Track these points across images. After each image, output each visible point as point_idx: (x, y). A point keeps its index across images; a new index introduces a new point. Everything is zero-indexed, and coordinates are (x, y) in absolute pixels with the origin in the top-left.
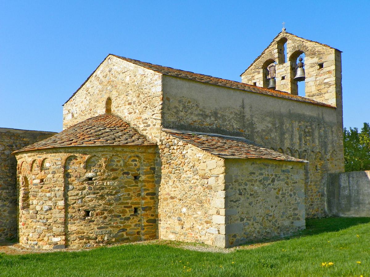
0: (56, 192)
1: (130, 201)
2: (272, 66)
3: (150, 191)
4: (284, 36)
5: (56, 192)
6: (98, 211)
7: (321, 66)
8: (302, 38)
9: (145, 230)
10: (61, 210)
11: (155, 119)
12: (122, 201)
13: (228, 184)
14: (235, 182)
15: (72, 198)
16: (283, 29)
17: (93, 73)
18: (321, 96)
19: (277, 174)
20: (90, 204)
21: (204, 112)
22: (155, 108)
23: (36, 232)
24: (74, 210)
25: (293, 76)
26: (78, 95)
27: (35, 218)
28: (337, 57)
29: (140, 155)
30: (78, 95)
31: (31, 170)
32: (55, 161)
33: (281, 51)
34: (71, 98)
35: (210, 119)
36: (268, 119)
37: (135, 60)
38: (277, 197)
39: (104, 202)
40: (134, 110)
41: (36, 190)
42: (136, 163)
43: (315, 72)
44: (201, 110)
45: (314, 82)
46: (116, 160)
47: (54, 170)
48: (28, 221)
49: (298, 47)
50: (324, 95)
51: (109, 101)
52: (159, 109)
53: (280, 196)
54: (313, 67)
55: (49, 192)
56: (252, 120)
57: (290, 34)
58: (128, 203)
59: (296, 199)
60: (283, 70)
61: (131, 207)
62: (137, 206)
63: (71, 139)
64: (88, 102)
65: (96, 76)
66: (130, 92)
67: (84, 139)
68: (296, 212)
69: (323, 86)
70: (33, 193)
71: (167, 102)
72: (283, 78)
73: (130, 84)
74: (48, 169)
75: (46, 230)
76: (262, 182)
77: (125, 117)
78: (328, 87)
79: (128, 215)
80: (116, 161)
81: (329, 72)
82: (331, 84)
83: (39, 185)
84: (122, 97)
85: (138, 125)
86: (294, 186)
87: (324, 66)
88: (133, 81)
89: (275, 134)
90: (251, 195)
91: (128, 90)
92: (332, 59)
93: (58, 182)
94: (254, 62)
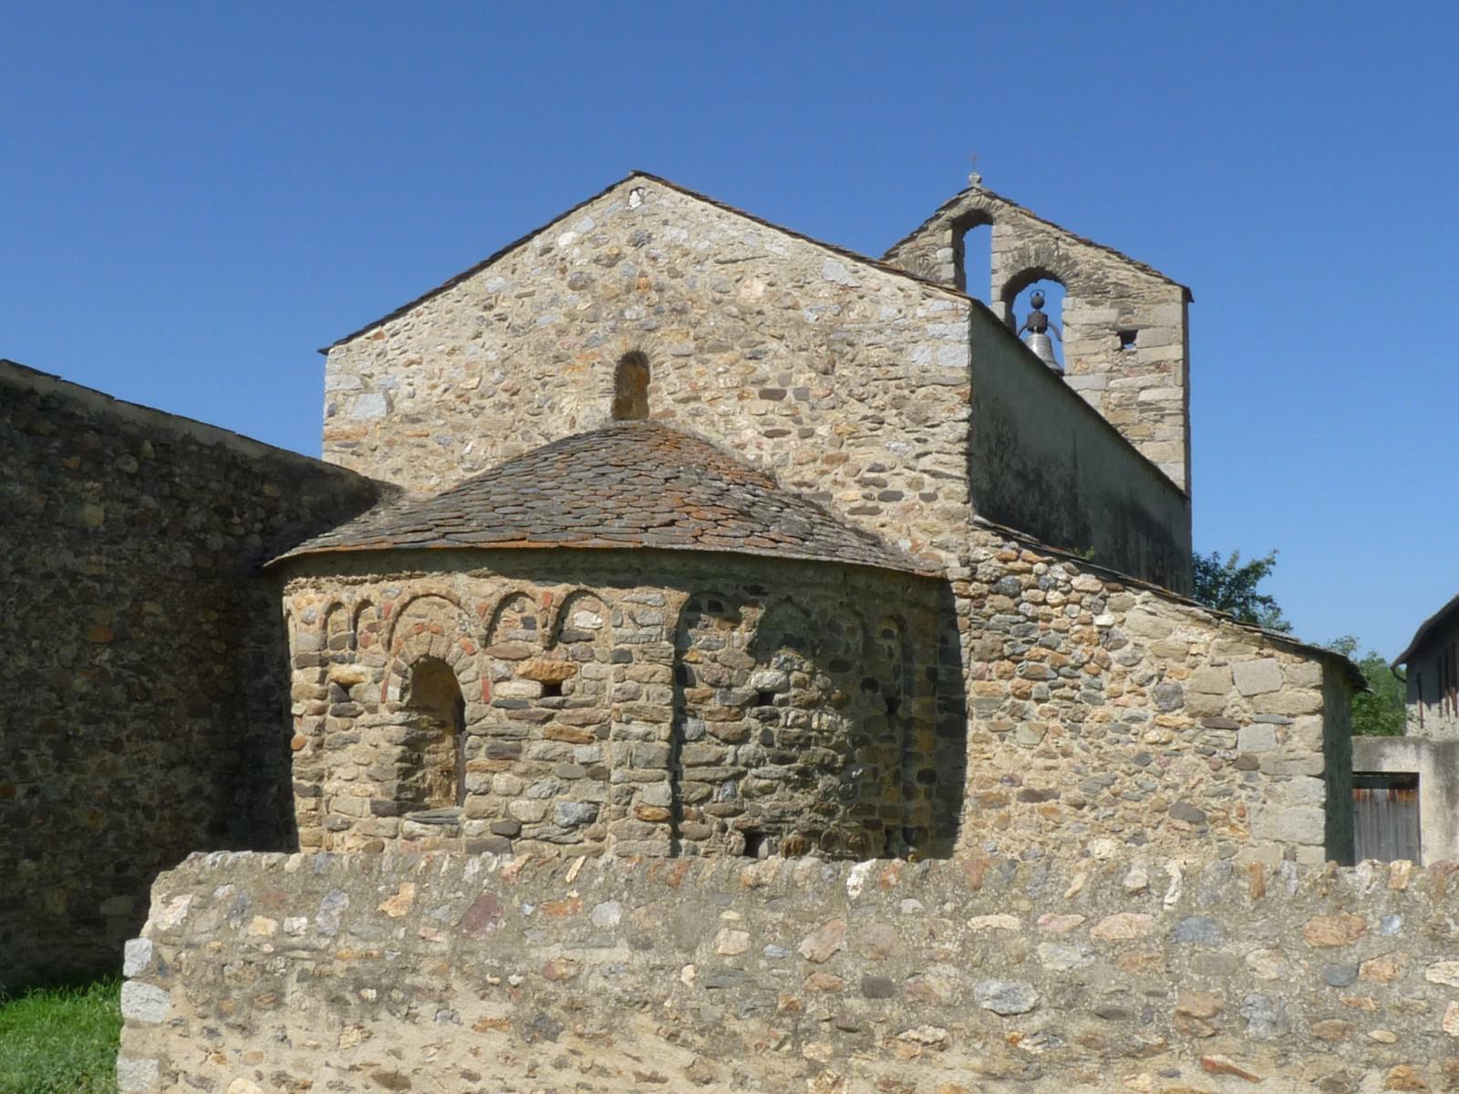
6: (791, 836)
7: (1127, 337)
8: (1054, 226)
10: (651, 825)
11: (935, 475)
15: (700, 772)
20: (765, 804)
22: (932, 430)
24: (705, 827)
34: (382, 323)
39: (811, 799)
43: (1102, 357)
49: (1037, 254)
54: (1097, 338)
55: (590, 741)
57: (1006, 201)
65: (546, 250)
69: (1135, 415)
74: (590, 640)
78: (1156, 422)
81: (1159, 366)
82: (1164, 409)
87: (1137, 341)
92: (1173, 323)
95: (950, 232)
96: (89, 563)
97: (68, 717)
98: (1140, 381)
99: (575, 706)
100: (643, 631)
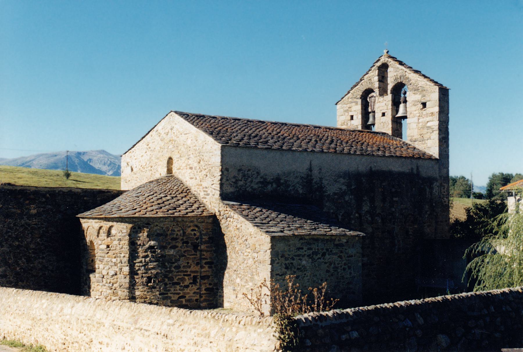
0: (121, 258)
1: (189, 270)
2: (372, 97)
3: (208, 260)
4: (385, 62)
5: (121, 258)
9: (204, 298)
11: (215, 189)
12: (182, 269)
13: (274, 259)
14: (281, 257)
16: (385, 51)
17: (154, 128)
18: (423, 142)
19: (328, 248)
21: (266, 179)
23: (102, 295)
25: (395, 113)
26: (138, 148)
27: (102, 281)
28: (442, 96)
29: (199, 225)
30: (138, 148)
31: (98, 236)
32: (121, 229)
33: (383, 78)
34: (130, 149)
35: (272, 185)
36: (342, 180)
37: (199, 116)
38: (328, 271)
40: (195, 175)
41: (103, 255)
42: (195, 232)
43: (417, 112)
44: (261, 178)
45: (416, 124)
46: (176, 230)
47: (120, 238)
48: (94, 284)
49: (400, 78)
50: (426, 142)
51: (170, 161)
52: (218, 180)
53: (332, 270)
55: (115, 257)
56: (322, 183)
58: (187, 272)
59: (350, 273)
60: (383, 104)
61: (190, 275)
62: (195, 274)
63: (135, 208)
64: (148, 158)
65: (157, 131)
66: (191, 156)
67: (147, 208)
68: (351, 286)
70: (99, 258)
71: (226, 172)
72: (384, 114)
73: (191, 148)
75: (112, 294)
76: (311, 256)
77: (186, 181)
78: (431, 133)
79: (187, 283)
80: (176, 230)
83: (105, 251)
84: (183, 159)
85: (199, 192)
86: (348, 260)
88: (194, 145)
89: (351, 197)
90: (298, 269)
91: (189, 153)
93: (123, 249)
94: (352, 89)
95: (377, 71)
96: (33, 222)
97: (29, 253)
98: (428, 119)
99: (113, 250)
100: (123, 234)
